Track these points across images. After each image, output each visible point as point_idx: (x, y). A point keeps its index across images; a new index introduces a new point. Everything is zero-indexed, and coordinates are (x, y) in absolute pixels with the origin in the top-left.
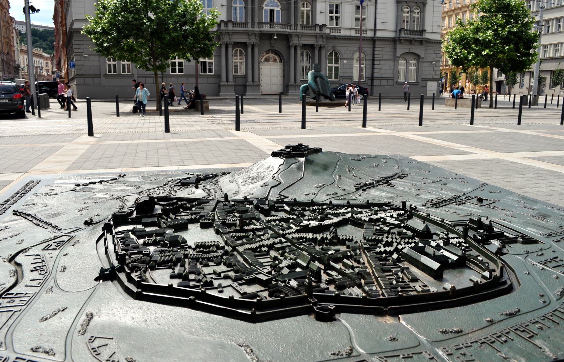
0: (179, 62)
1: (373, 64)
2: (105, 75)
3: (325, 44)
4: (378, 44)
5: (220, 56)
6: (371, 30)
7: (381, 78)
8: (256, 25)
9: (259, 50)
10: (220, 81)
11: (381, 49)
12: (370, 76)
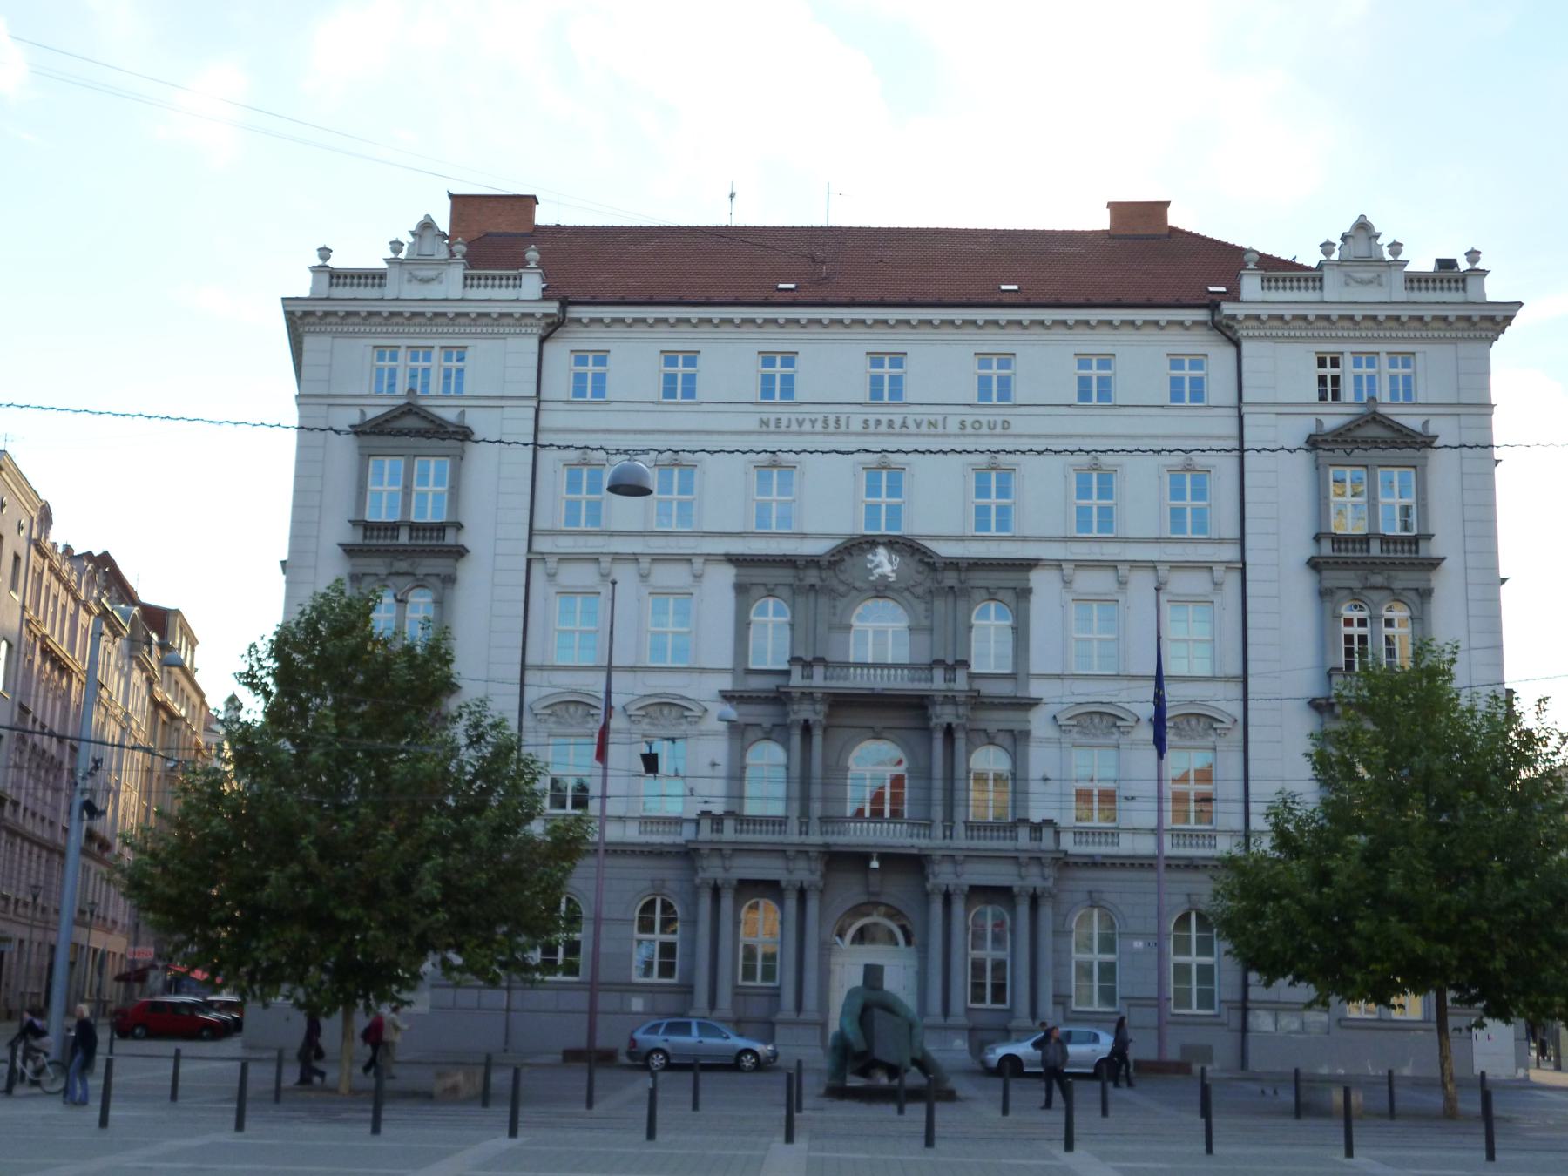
0: (1199, 967)
3: (1050, 883)
5: (692, 922)
6: (1232, 833)
8: (815, 826)
12: (1237, 996)
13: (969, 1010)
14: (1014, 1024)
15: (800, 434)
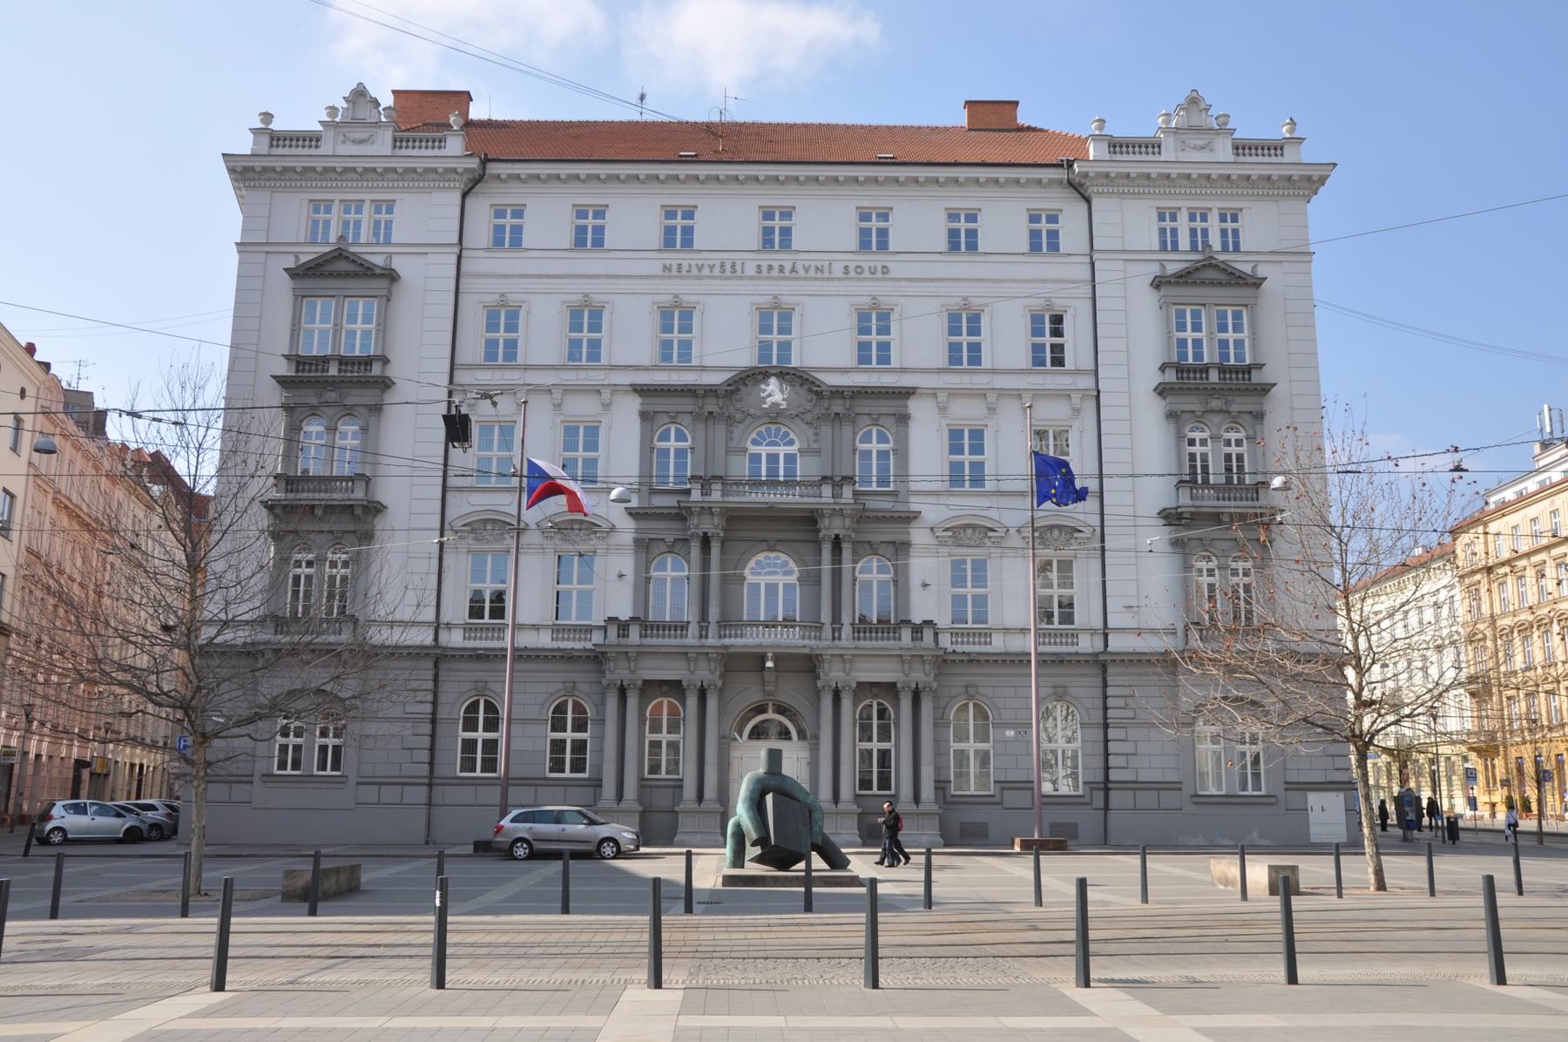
2: (268, 776)
6: (1093, 631)
7: (1134, 786)
8: (713, 630)
10: (597, 797)
11: (1125, 691)
12: (1100, 778)
15: (699, 278)
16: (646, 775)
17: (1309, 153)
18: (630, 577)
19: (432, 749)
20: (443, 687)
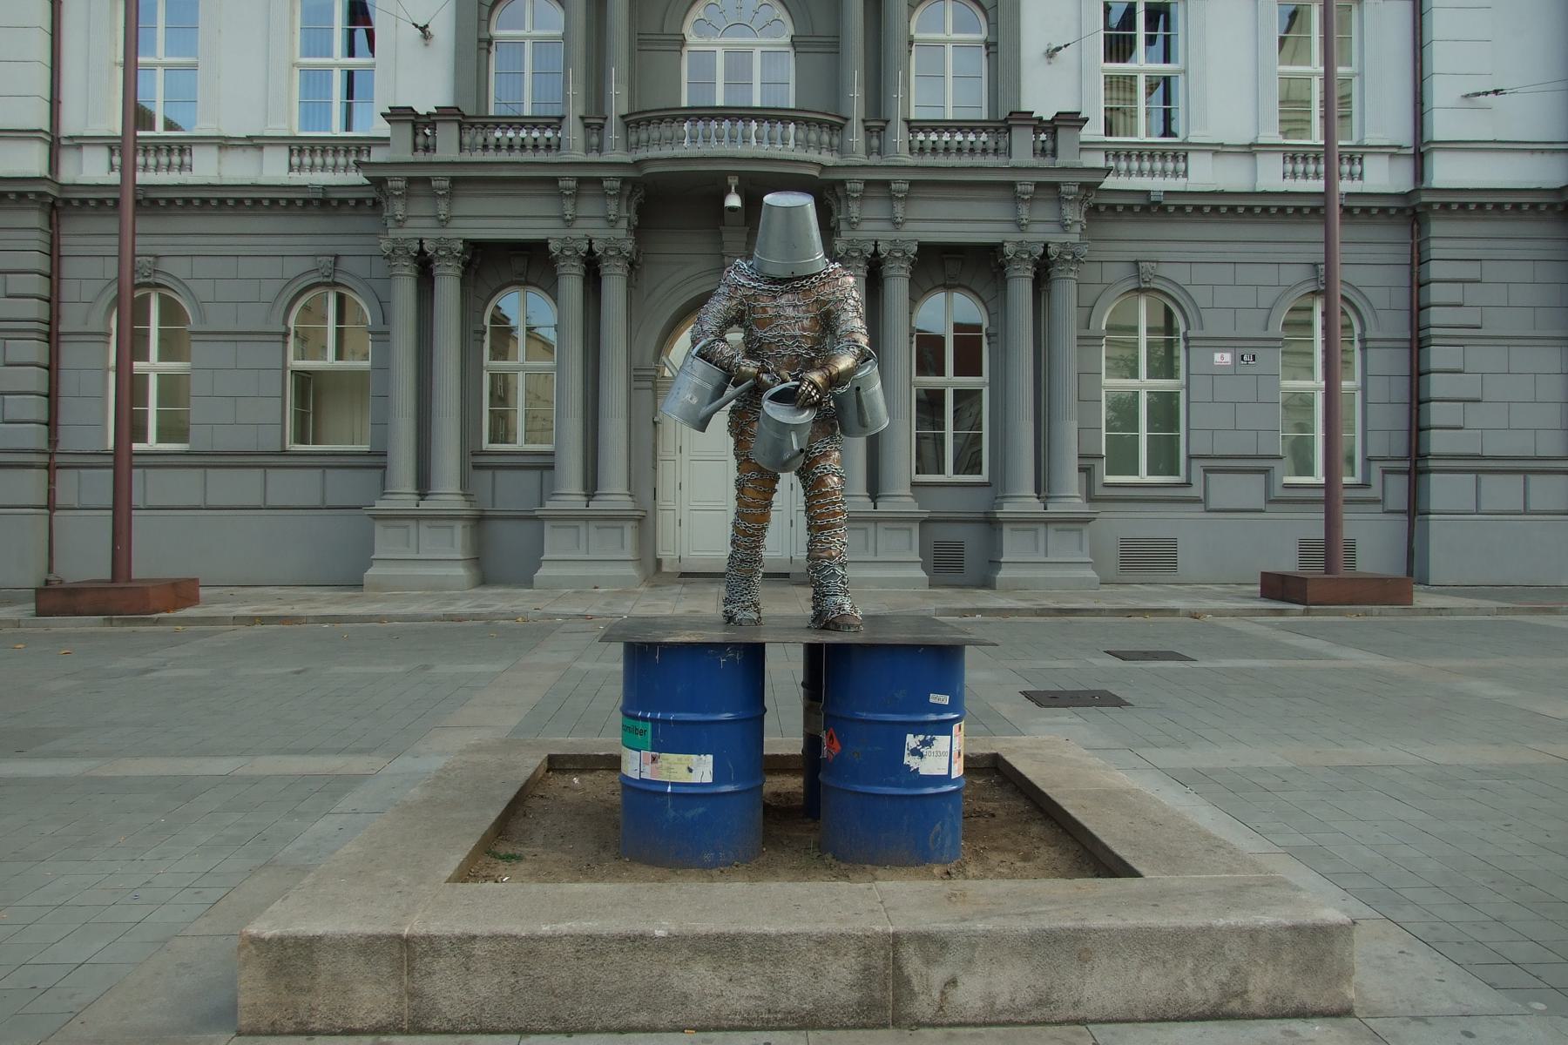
1: (1418, 374)
3: (1073, 237)
4: (1444, 237)
6: (1392, 152)
7: (1478, 465)
8: (613, 133)
9: (631, 286)
12: (1400, 446)
13: (914, 485)
14: (1009, 508)
16: (486, 445)
17: (1083, 115)
18: (444, 31)
19: (52, 396)
20: (69, 268)
